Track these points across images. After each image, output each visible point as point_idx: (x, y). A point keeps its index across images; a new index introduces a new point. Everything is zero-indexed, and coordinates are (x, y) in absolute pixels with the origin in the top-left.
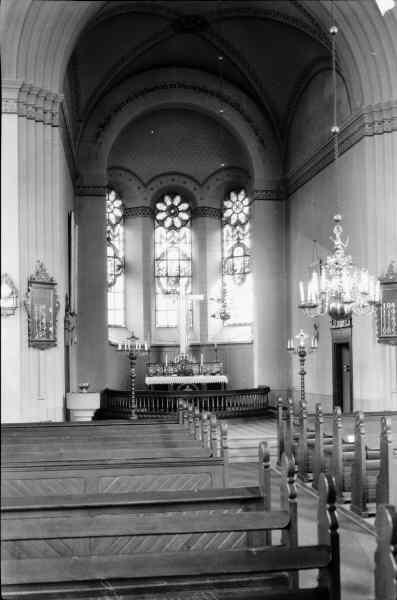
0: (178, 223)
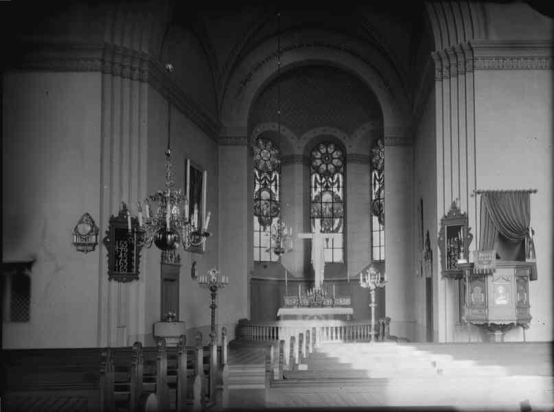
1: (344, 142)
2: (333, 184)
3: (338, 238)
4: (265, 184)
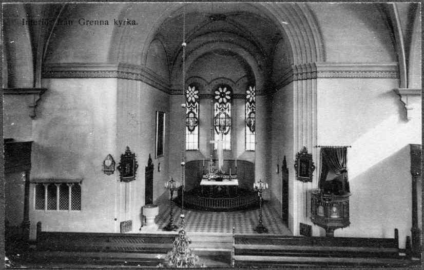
0: (225, 100)
1: (232, 88)
2: (226, 109)
3: (228, 137)
4: (191, 110)
